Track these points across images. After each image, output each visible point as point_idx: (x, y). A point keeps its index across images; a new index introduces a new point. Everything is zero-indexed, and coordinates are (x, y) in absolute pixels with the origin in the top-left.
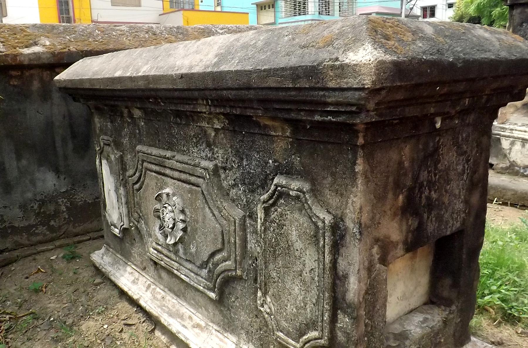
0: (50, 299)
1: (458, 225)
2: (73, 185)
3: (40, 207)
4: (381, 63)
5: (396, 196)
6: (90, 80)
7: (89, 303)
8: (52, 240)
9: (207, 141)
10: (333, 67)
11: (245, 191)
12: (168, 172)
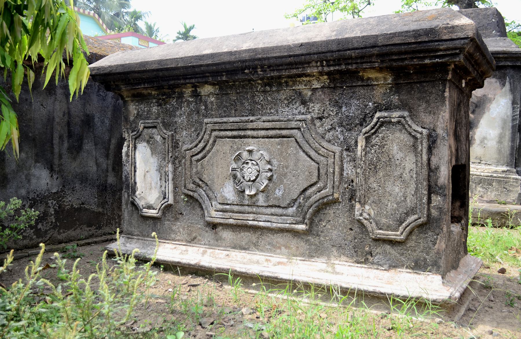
10: (446, 28)
12: (249, 133)
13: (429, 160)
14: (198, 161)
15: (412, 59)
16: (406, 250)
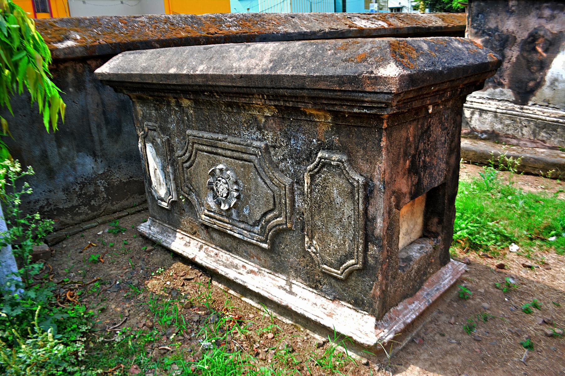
0: (110, 267)
1: (442, 179)
2: (109, 167)
3: (81, 189)
4: (402, 77)
5: (405, 161)
6: (140, 75)
7: (147, 267)
8: (94, 218)
9: (258, 126)
10: (369, 78)
11: (292, 164)
12: (220, 151)
13: (366, 210)
14: (188, 168)
15: (342, 105)
16: (347, 287)
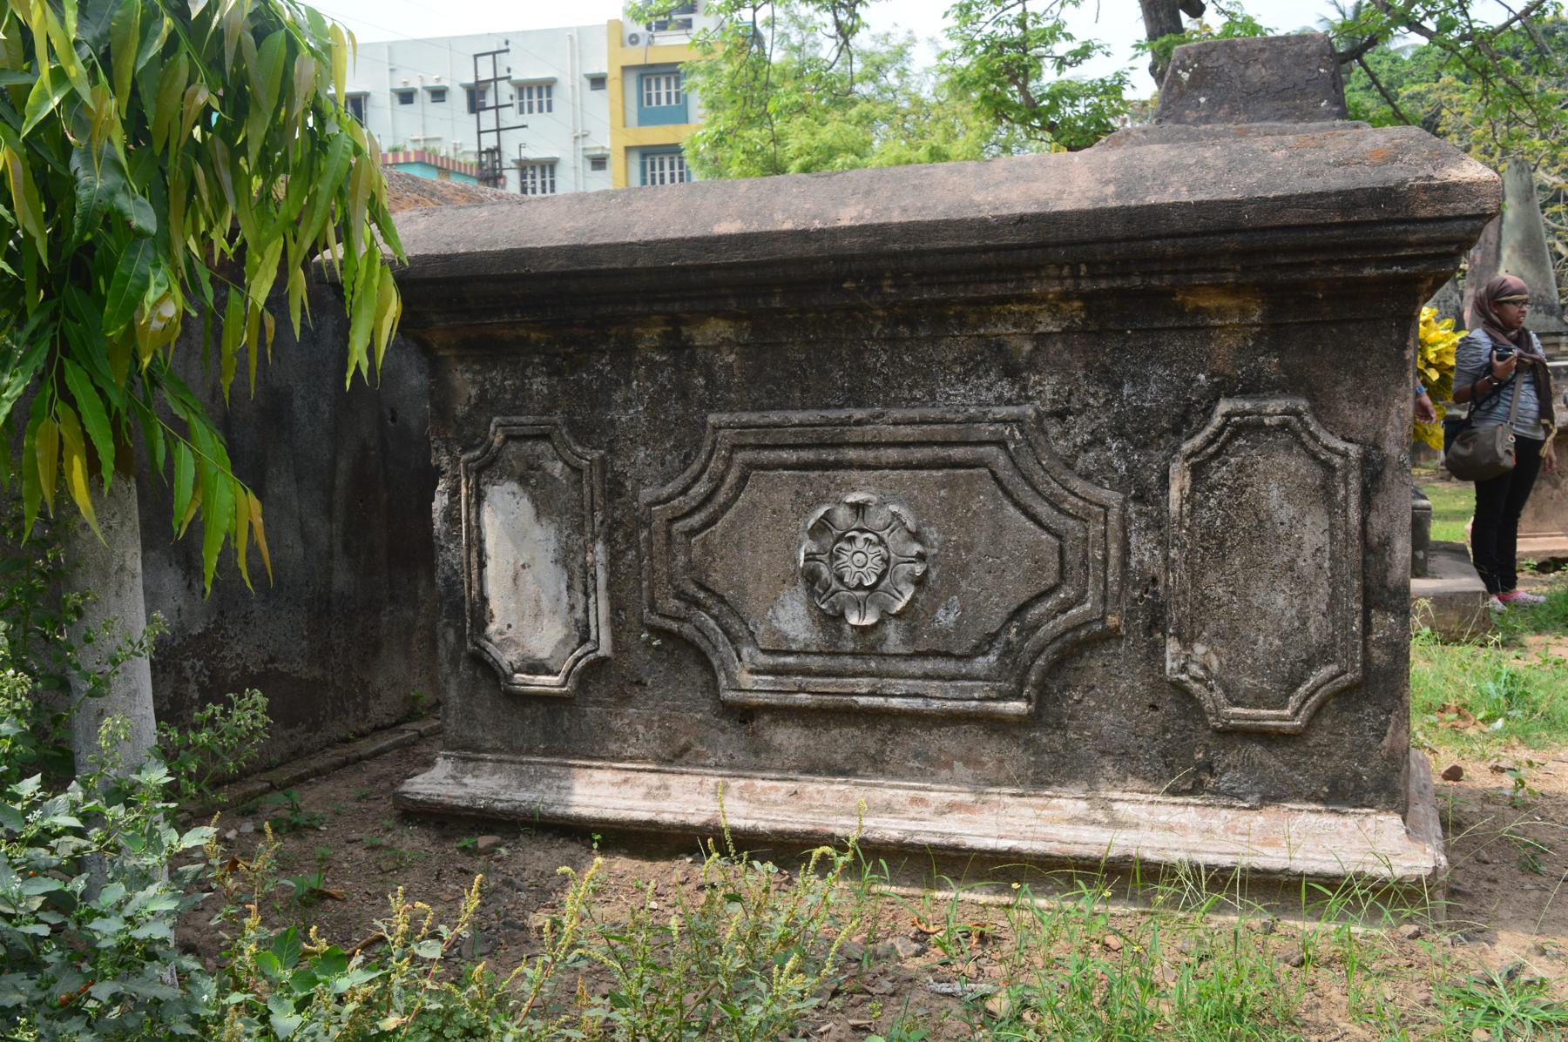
10: (1426, 189)
12: (851, 454)
16: (1305, 754)
